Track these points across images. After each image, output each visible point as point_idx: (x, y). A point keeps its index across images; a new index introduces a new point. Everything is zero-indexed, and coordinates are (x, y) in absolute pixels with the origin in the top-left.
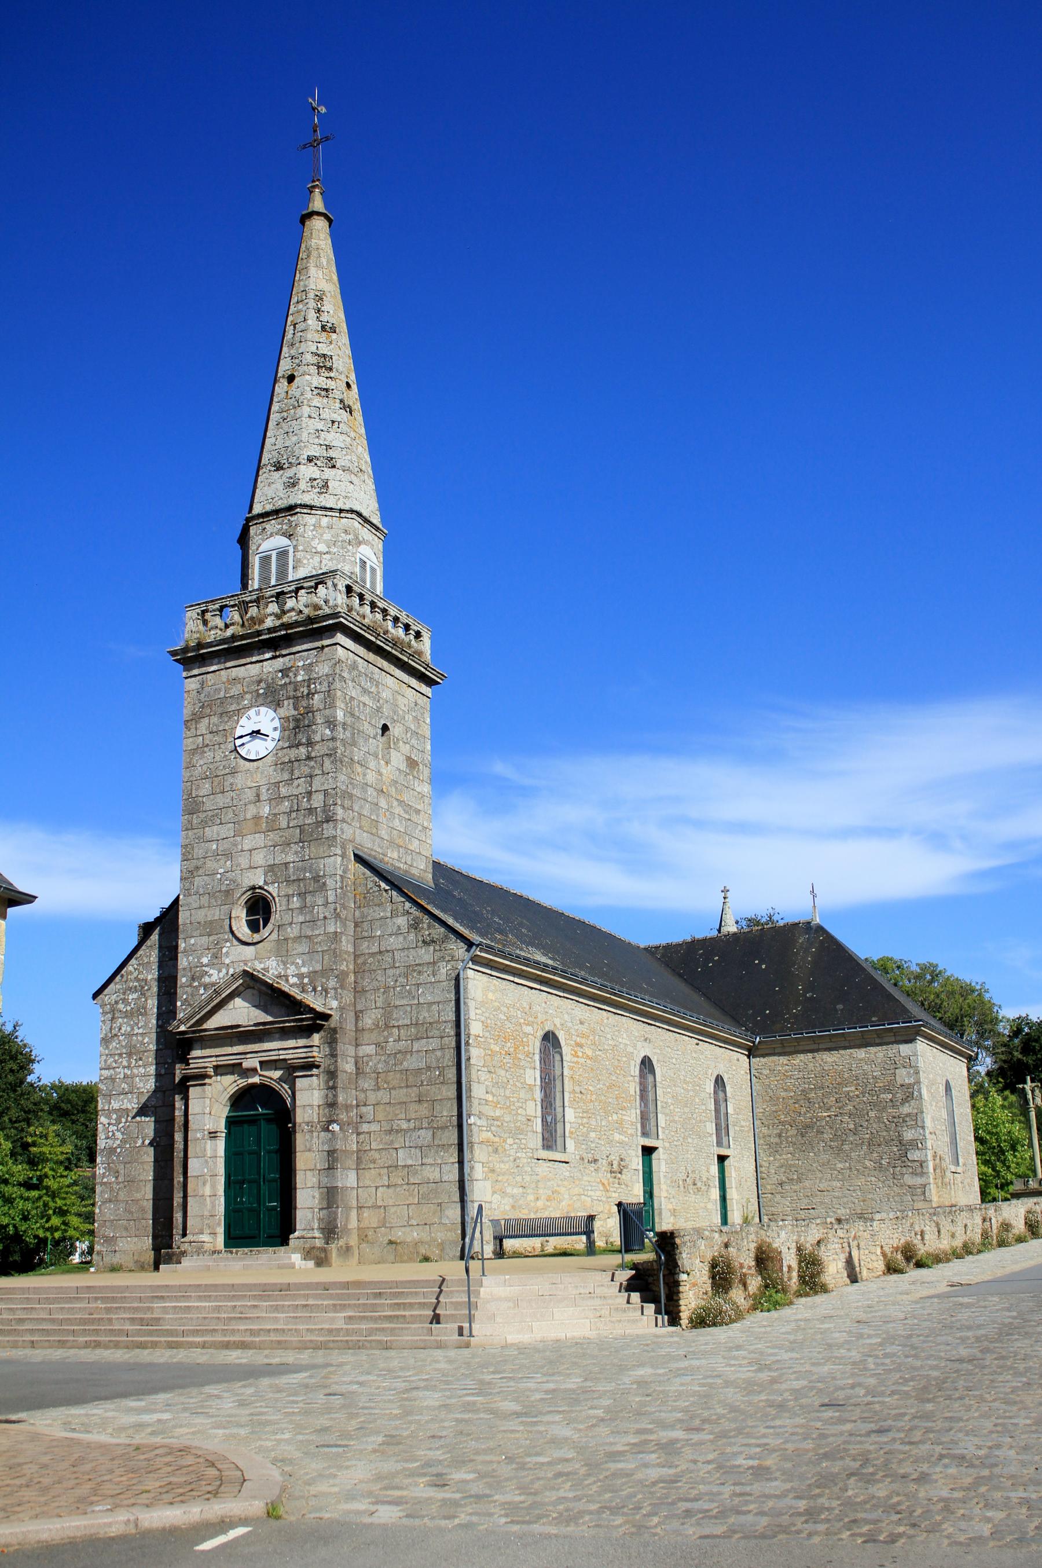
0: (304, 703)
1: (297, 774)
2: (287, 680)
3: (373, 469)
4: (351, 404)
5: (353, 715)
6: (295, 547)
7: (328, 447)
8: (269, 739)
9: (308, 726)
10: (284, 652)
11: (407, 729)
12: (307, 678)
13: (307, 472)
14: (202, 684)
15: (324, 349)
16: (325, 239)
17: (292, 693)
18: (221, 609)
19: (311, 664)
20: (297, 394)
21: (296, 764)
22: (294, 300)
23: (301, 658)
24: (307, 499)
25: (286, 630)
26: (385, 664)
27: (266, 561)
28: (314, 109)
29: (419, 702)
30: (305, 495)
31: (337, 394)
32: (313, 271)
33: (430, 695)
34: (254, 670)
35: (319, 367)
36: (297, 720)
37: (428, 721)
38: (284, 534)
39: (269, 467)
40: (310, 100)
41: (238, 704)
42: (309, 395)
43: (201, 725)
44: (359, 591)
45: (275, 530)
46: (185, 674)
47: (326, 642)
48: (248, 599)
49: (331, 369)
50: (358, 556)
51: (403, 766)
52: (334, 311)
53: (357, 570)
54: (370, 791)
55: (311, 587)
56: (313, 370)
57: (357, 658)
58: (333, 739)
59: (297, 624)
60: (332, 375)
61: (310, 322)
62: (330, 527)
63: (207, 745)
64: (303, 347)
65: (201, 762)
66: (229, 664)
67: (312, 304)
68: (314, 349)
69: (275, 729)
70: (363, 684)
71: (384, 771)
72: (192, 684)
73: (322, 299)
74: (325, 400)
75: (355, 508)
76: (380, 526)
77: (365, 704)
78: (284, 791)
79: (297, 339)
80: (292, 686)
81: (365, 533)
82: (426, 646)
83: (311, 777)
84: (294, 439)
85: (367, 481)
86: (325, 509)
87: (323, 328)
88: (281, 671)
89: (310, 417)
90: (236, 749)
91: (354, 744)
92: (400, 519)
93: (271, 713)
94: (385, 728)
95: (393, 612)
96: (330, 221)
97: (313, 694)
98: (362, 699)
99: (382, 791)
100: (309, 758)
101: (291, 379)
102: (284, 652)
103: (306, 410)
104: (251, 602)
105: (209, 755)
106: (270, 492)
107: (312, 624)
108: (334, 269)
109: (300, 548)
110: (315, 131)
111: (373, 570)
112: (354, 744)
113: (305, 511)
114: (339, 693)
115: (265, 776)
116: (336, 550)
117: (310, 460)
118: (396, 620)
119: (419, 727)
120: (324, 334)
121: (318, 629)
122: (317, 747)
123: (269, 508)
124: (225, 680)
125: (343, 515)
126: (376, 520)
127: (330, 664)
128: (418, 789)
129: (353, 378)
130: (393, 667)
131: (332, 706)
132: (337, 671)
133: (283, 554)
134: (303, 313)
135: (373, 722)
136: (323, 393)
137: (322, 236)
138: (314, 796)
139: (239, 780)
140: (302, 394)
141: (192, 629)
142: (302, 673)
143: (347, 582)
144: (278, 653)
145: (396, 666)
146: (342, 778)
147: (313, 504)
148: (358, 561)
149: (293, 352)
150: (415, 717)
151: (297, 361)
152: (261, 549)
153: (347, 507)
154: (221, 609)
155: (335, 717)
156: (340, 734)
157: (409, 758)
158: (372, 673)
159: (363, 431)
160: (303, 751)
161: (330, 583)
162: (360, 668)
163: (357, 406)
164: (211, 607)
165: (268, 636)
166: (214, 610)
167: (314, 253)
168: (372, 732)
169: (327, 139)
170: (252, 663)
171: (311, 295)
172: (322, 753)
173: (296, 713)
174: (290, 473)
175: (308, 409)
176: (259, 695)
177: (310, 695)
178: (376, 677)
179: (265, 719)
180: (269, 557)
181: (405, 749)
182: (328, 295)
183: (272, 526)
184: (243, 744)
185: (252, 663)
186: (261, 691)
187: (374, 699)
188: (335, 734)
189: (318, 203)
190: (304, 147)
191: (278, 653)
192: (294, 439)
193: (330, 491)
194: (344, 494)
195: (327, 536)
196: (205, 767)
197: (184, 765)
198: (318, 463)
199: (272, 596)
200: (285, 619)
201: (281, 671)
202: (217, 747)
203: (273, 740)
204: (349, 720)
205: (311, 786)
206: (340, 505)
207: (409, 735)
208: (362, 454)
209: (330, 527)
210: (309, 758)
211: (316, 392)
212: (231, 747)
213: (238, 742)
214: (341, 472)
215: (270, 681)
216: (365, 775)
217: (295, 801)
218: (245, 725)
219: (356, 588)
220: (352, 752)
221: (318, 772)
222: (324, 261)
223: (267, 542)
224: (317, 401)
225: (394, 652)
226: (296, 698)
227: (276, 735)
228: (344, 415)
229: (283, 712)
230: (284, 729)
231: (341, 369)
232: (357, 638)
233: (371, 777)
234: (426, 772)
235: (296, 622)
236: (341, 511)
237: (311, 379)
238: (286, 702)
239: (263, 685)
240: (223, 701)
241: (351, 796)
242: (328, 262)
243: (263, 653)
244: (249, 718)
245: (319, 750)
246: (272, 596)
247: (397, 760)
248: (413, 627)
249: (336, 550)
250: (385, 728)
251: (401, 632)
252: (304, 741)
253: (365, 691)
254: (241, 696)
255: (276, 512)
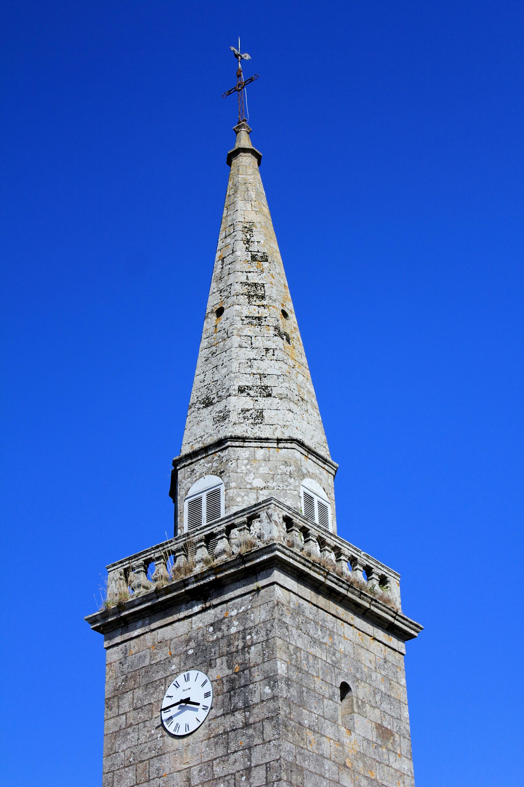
0: (239, 659)
1: (233, 747)
2: (219, 634)
3: (318, 399)
4: (288, 332)
5: (299, 669)
6: (227, 485)
7: (262, 376)
8: (200, 707)
9: (245, 686)
10: (215, 602)
11: (375, 691)
12: (241, 628)
13: (238, 403)
14: (125, 653)
15: (254, 278)
16: (253, 173)
17: (225, 650)
18: (148, 562)
19: (245, 612)
20: (226, 326)
21: (232, 735)
22: (222, 235)
23: (235, 607)
24: (238, 431)
25: (215, 574)
26: (341, 611)
27: (195, 505)
28: (237, 56)
29: (390, 658)
30: (236, 427)
31: (271, 322)
32: (240, 204)
33: (403, 651)
34: (182, 628)
35: (249, 296)
36: (231, 681)
37: (403, 682)
38: (215, 473)
39: (198, 405)
40: (233, 48)
41: (165, 670)
42: (239, 325)
43: (125, 701)
44: (302, 524)
45: (205, 470)
46: (106, 644)
47: (262, 583)
48: (174, 548)
49: (263, 297)
50: (302, 490)
51: (373, 736)
52: (266, 240)
53: (301, 505)
54: (328, 765)
55: (244, 523)
56: (243, 299)
57: (301, 601)
58: (274, 698)
59: (227, 565)
60: (264, 302)
61: (238, 253)
62: (267, 460)
63: (131, 725)
64: (232, 279)
65: (124, 747)
66: (154, 626)
67: (240, 235)
68: (244, 279)
69: (207, 695)
70: (311, 632)
71: (346, 740)
72: (114, 655)
73: (251, 230)
74: (258, 329)
75: (295, 437)
76: (330, 459)
77: (315, 657)
78: (218, 770)
79: (226, 272)
80: (225, 641)
81: (309, 465)
82: (394, 592)
83: (250, 748)
84: (224, 371)
85: (311, 411)
86: (260, 439)
87: (254, 258)
88: (212, 625)
89: (240, 346)
90: (162, 725)
91: (302, 704)
92: (352, 446)
93: (202, 677)
94: (345, 688)
95: (347, 551)
96: (259, 158)
97: (249, 647)
98: (312, 650)
99: (345, 765)
100: (247, 725)
101: (220, 312)
102: (215, 602)
103: (236, 340)
104: (178, 550)
105: (133, 736)
106: (198, 429)
107: (244, 562)
108: (264, 202)
109: (233, 485)
110: (239, 76)
111: (323, 508)
112: (302, 704)
113: (237, 444)
114: (279, 642)
115: (199, 751)
116: (274, 484)
117: (241, 390)
118: (353, 561)
119: (391, 688)
120: (255, 264)
121: (252, 568)
122: (256, 711)
123: (197, 447)
124: (150, 644)
125: (281, 445)
126: (324, 452)
127: (268, 608)
128: (396, 766)
129: (290, 307)
130: (351, 615)
131: (272, 658)
132: (276, 615)
133: (214, 495)
134: (231, 247)
135: (328, 679)
136: (255, 322)
137: (250, 171)
138: (254, 773)
139: (167, 764)
140: (232, 325)
141: (116, 589)
142: (236, 623)
143: (285, 513)
144: (208, 604)
145: (355, 614)
146: (287, 746)
147: (245, 435)
148: (302, 495)
149: (221, 286)
150: (386, 678)
151: (226, 293)
152: (190, 494)
153: (286, 437)
154: (148, 562)
155: (275, 671)
156: (283, 690)
157: (379, 727)
158: (324, 621)
159: (304, 360)
160: (239, 716)
161: (263, 515)
162: (307, 613)
163: (296, 336)
164: (135, 563)
165: (195, 585)
166: (138, 567)
167: (242, 188)
168: (326, 691)
169: (251, 80)
170: (179, 620)
171: (239, 227)
172: (262, 716)
173: (230, 672)
174: (219, 407)
175: (239, 339)
176: (188, 657)
177: (246, 648)
178: (330, 625)
179: (195, 685)
180: (200, 500)
181: (375, 715)
182: (258, 226)
183: (201, 465)
184: (171, 718)
185: (179, 620)
186: (191, 652)
187: (328, 652)
188: (276, 691)
189: (244, 140)
190: (230, 93)
191: (208, 604)
192: (224, 371)
193: (266, 421)
194: (282, 423)
195: (264, 470)
196: (128, 753)
197: (105, 752)
198: (252, 393)
199: (200, 541)
200: (217, 562)
201: (212, 625)
202: (141, 725)
203: (205, 708)
204: (294, 675)
205: (250, 760)
206: (278, 435)
207: (378, 698)
208: (303, 382)
209: (267, 460)
210: (247, 725)
211: (247, 321)
212: (158, 722)
213: (165, 716)
214: (277, 400)
215: (200, 638)
216: (319, 744)
217: (232, 782)
218: (174, 694)
219: (296, 520)
220: (300, 715)
221: (257, 741)
222: (253, 194)
223: (197, 484)
224: (248, 331)
225: (350, 595)
226: (229, 654)
227: (208, 701)
228: (280, 342)
229: (215, 673)
230: (217, 694)
231: (274, 297)
232: (301, 577)
233: (328, 747)
234: (405, 745)
235: (227, 563)
236: (279, 441)
237: (240, 308)
238: (218, 661)
239: (192, 644)
240: (147, 670)
241: (301, 770)
242: (257, 194)
243: (192, 607)
244: (177, 686)
245: (258, 713)
246: (200, 541)
247: (364, 727)
248: (375, 570)
249: (274, 484)
250: (345, 688)
251: (360, 576)
252: (240, 704)
253: (315, 641)
254: (168, 661)
255: (205, 450)
